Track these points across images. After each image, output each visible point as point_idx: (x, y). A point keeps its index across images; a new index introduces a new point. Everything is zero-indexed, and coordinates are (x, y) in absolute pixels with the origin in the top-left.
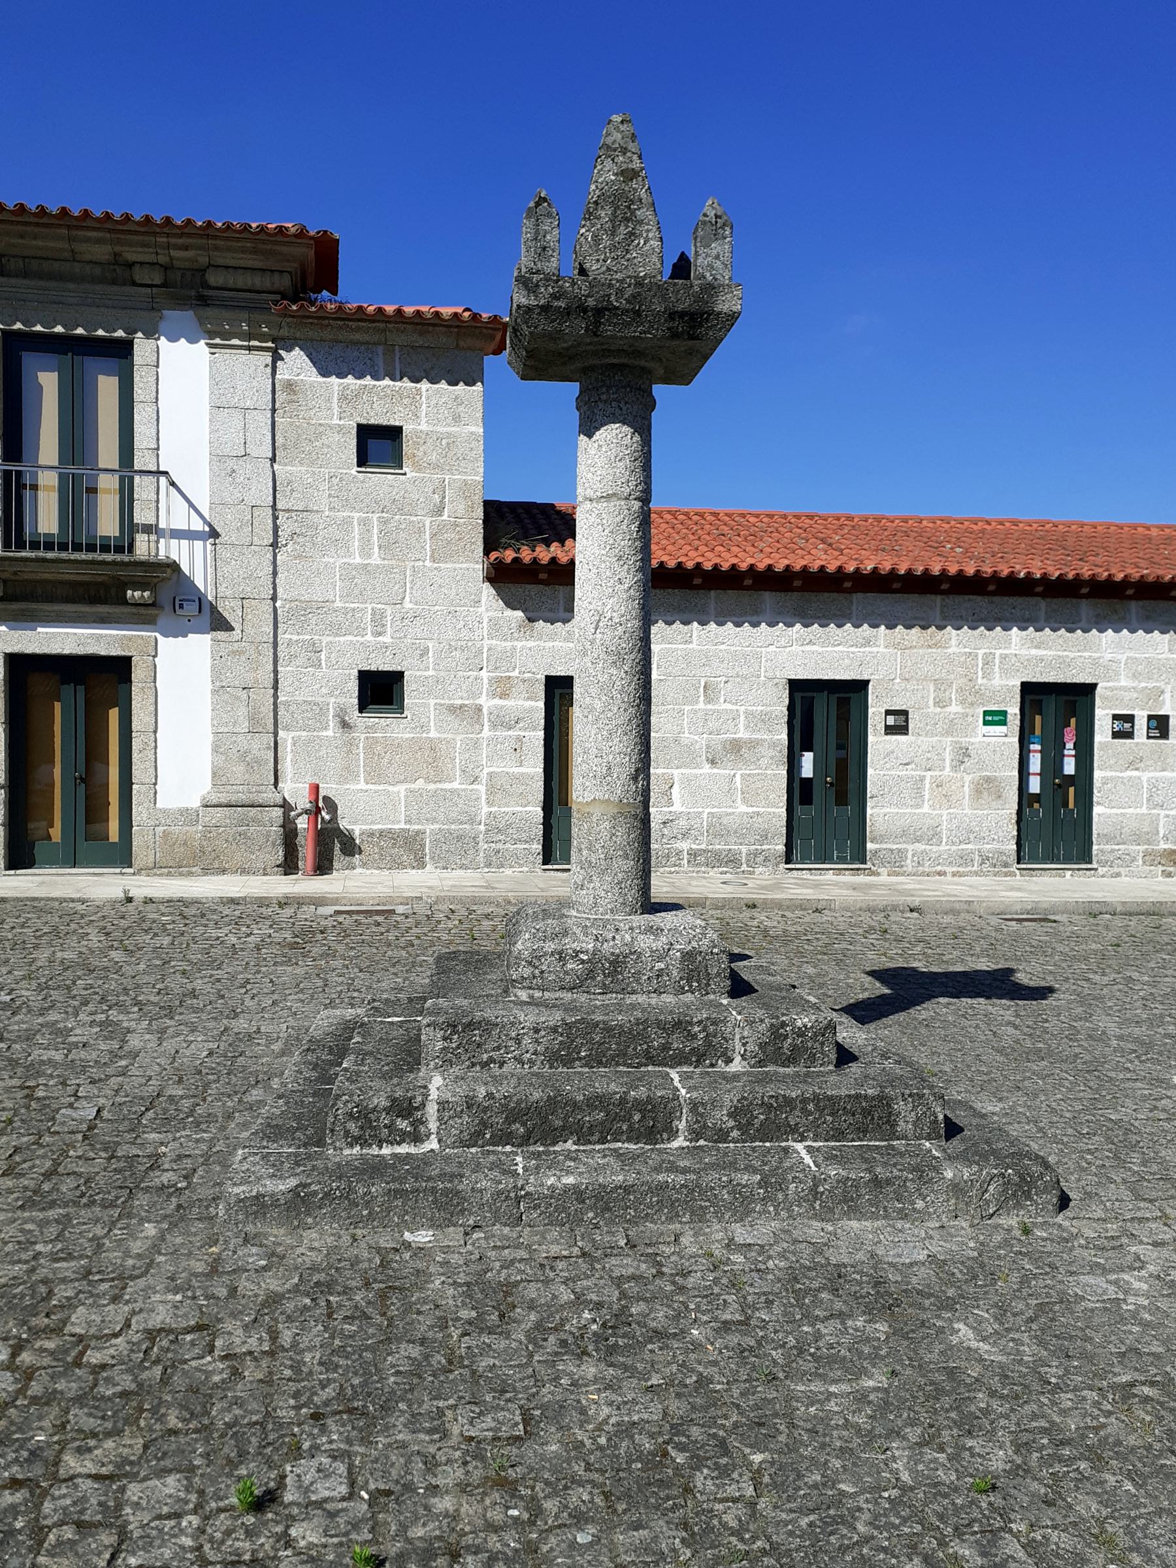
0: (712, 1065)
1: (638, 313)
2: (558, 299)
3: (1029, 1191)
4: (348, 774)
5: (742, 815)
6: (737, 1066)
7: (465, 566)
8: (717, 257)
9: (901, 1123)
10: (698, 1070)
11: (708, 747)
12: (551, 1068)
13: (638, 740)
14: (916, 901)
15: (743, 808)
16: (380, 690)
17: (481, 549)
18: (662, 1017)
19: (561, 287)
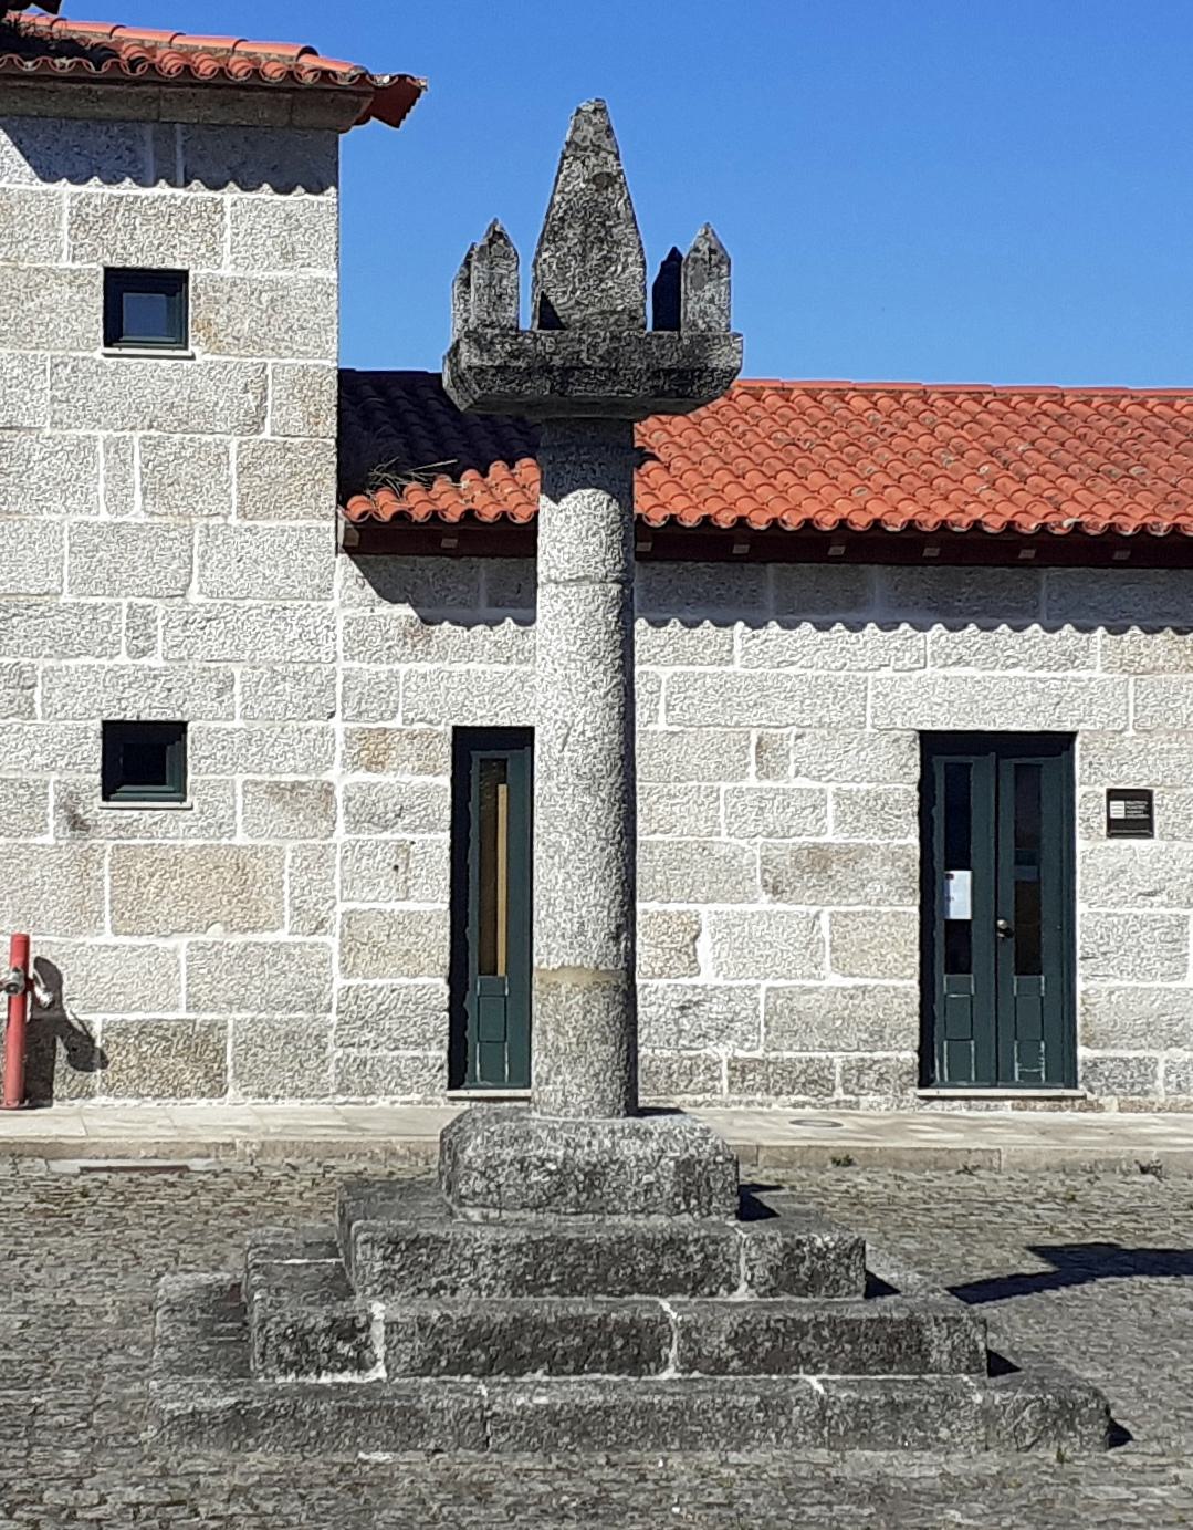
0: (712, 1294)
1: (615, 372)
2: (517, 358)
3: (1072, 1420)
4: (82, 916)
5: (834, 991)
6: (742, 1294)
7: (300, 523)
8: (711, 301)
9: (935, 1354)
10: (694, 1300)
11: (766, 860)
12: (514, 1295)
13: (618, 887)
14: (1152, 1154)
15: (835, 980)
16: (142, 758)
17: (333, 493)
18: (650, 1235)
19: (521, 344)
